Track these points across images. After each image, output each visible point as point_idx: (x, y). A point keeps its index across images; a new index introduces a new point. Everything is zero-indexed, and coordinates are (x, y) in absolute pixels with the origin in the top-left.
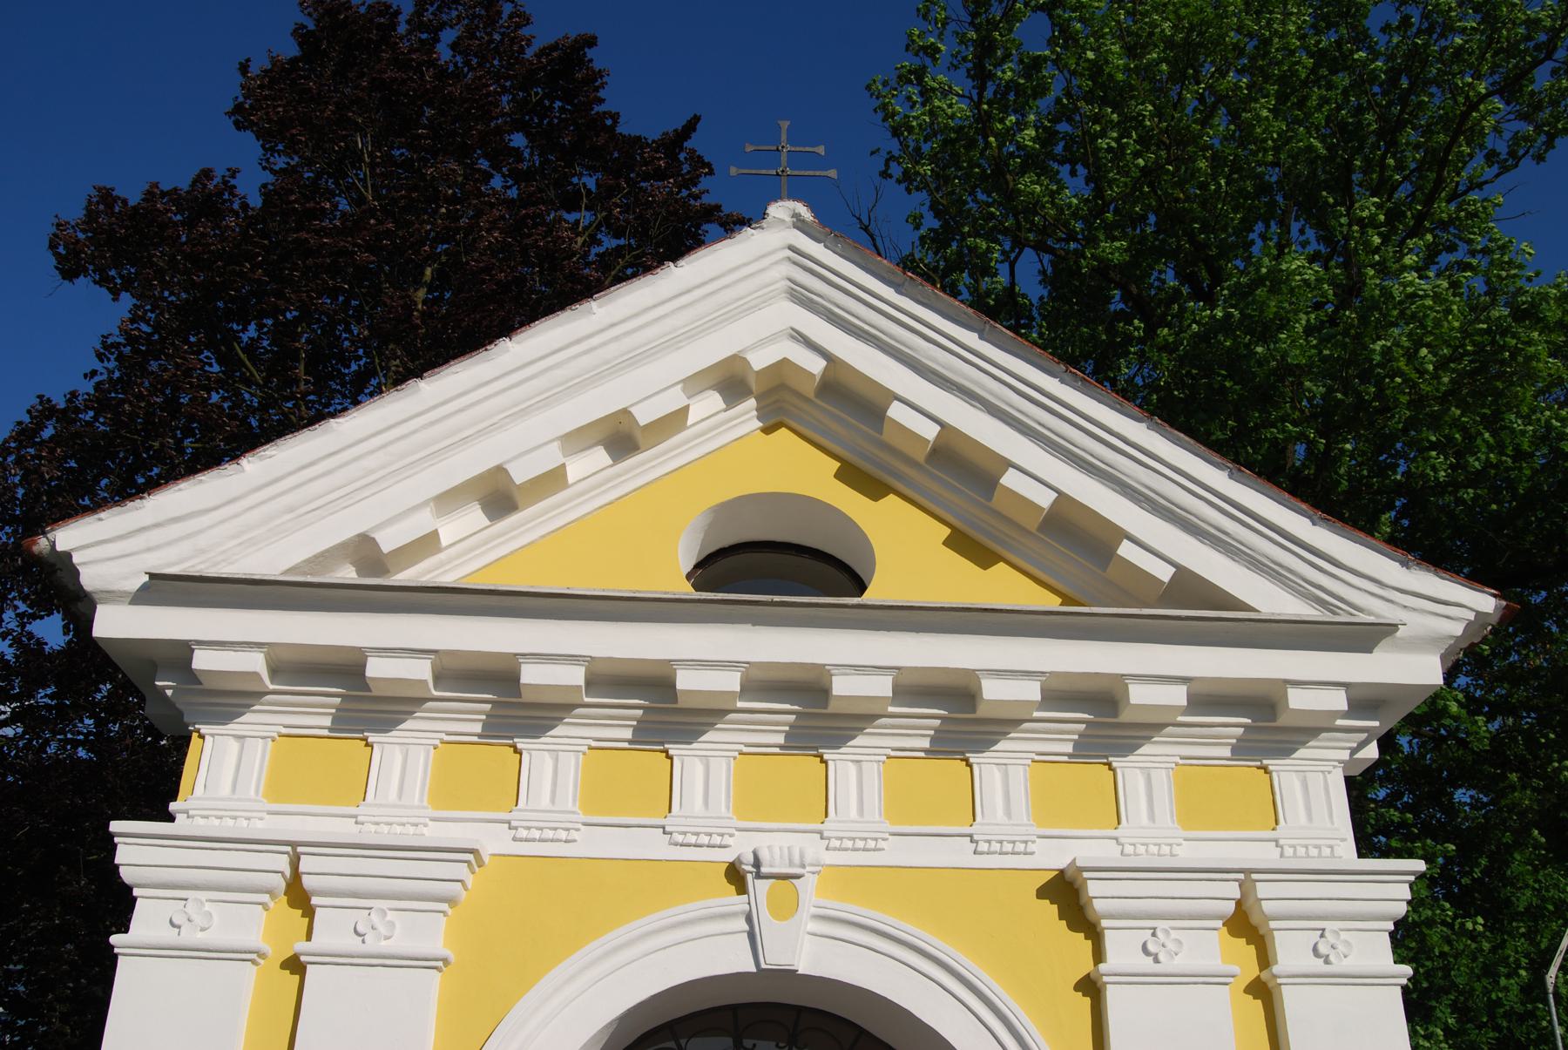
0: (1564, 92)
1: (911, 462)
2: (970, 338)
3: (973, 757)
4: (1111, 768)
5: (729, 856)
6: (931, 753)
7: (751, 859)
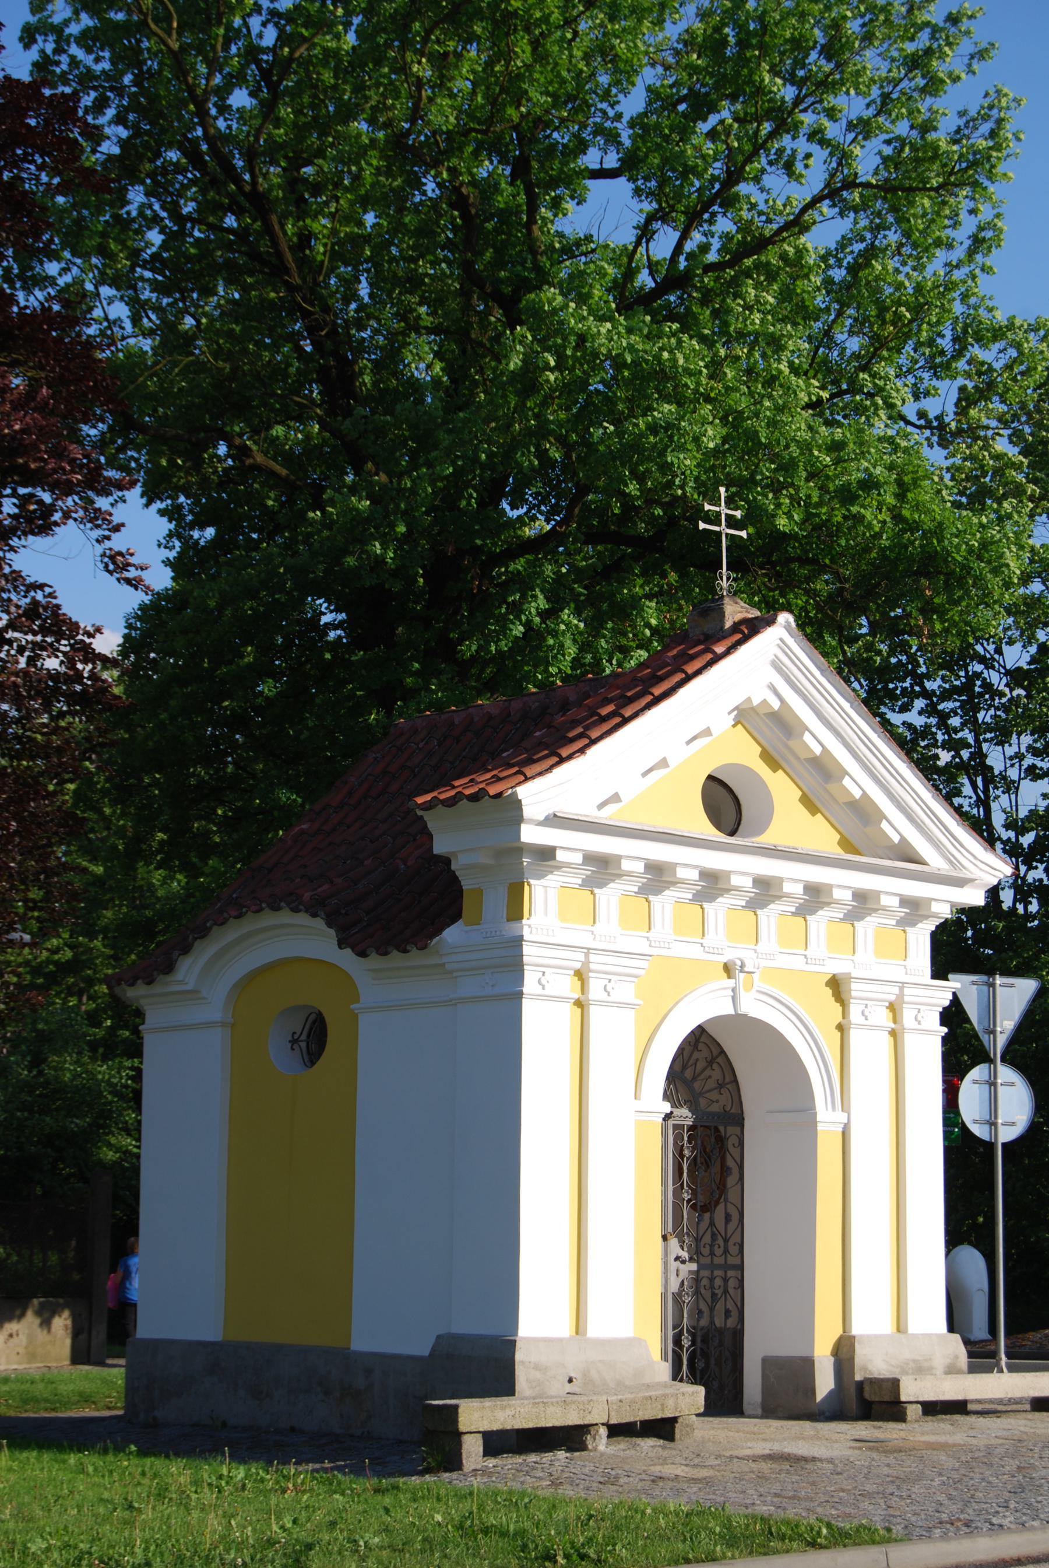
0: (1043, 442)
1: (798, 758)
2: (846, 705)
3: (596, 891)
4: (592, 892)
5: (724, 959)
6: (794, 914)
7: (739, 963)
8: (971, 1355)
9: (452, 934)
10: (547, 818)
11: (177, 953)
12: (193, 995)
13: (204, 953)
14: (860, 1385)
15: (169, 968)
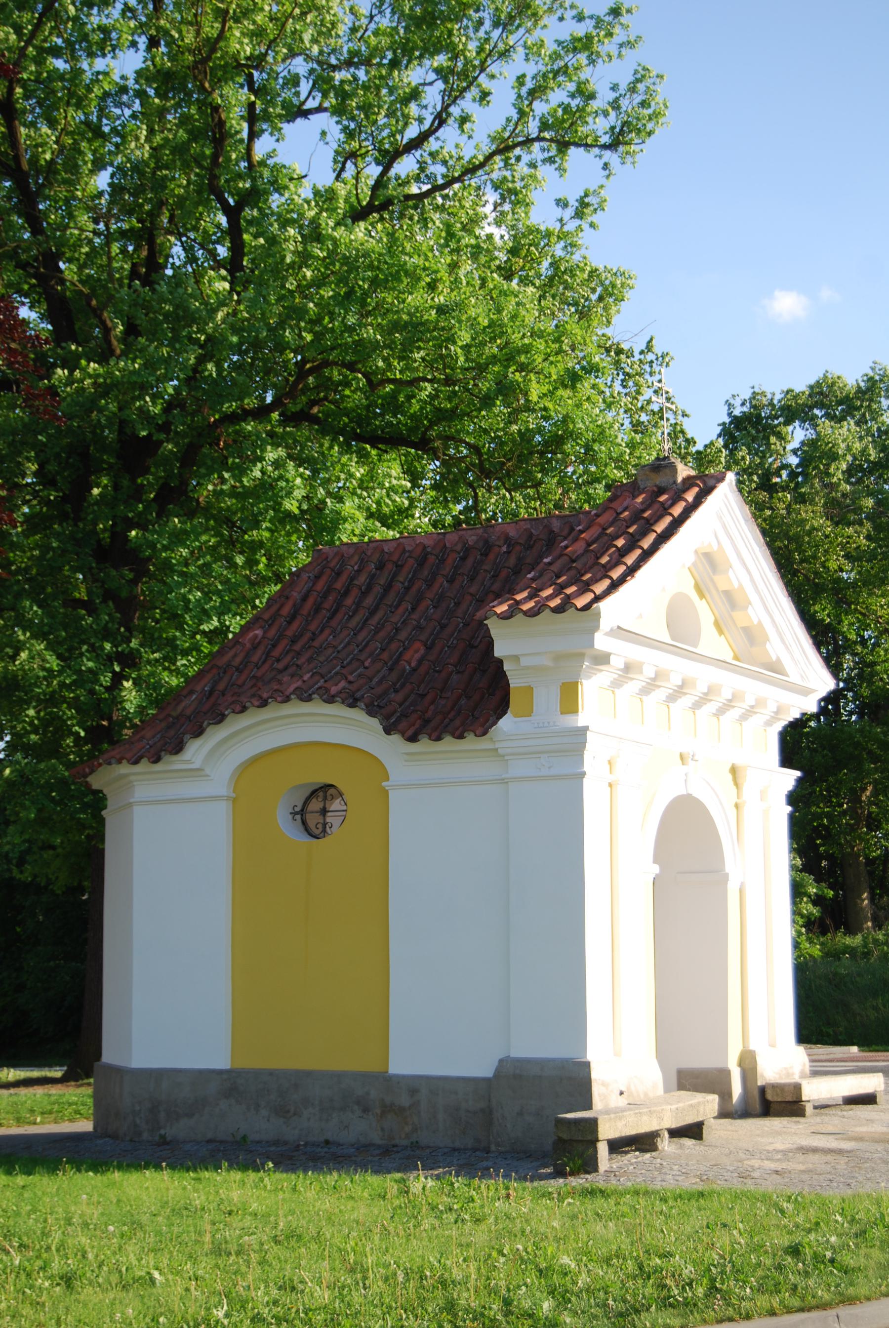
2: (757, 549)
8: (812, 1061)
9: (506, 723)
10: (612, 630)
11: (188, 736)
12: (197, 773)
13: (215, 735)
14: (763, 1090)
15: (178, 748)
